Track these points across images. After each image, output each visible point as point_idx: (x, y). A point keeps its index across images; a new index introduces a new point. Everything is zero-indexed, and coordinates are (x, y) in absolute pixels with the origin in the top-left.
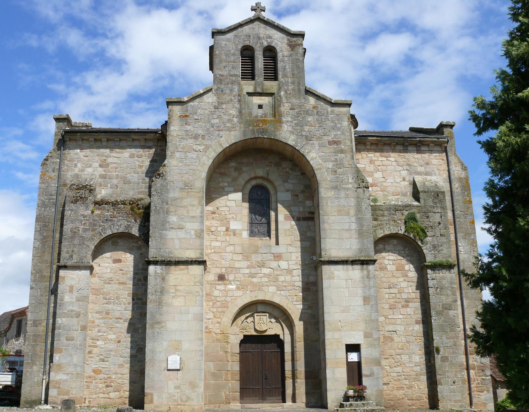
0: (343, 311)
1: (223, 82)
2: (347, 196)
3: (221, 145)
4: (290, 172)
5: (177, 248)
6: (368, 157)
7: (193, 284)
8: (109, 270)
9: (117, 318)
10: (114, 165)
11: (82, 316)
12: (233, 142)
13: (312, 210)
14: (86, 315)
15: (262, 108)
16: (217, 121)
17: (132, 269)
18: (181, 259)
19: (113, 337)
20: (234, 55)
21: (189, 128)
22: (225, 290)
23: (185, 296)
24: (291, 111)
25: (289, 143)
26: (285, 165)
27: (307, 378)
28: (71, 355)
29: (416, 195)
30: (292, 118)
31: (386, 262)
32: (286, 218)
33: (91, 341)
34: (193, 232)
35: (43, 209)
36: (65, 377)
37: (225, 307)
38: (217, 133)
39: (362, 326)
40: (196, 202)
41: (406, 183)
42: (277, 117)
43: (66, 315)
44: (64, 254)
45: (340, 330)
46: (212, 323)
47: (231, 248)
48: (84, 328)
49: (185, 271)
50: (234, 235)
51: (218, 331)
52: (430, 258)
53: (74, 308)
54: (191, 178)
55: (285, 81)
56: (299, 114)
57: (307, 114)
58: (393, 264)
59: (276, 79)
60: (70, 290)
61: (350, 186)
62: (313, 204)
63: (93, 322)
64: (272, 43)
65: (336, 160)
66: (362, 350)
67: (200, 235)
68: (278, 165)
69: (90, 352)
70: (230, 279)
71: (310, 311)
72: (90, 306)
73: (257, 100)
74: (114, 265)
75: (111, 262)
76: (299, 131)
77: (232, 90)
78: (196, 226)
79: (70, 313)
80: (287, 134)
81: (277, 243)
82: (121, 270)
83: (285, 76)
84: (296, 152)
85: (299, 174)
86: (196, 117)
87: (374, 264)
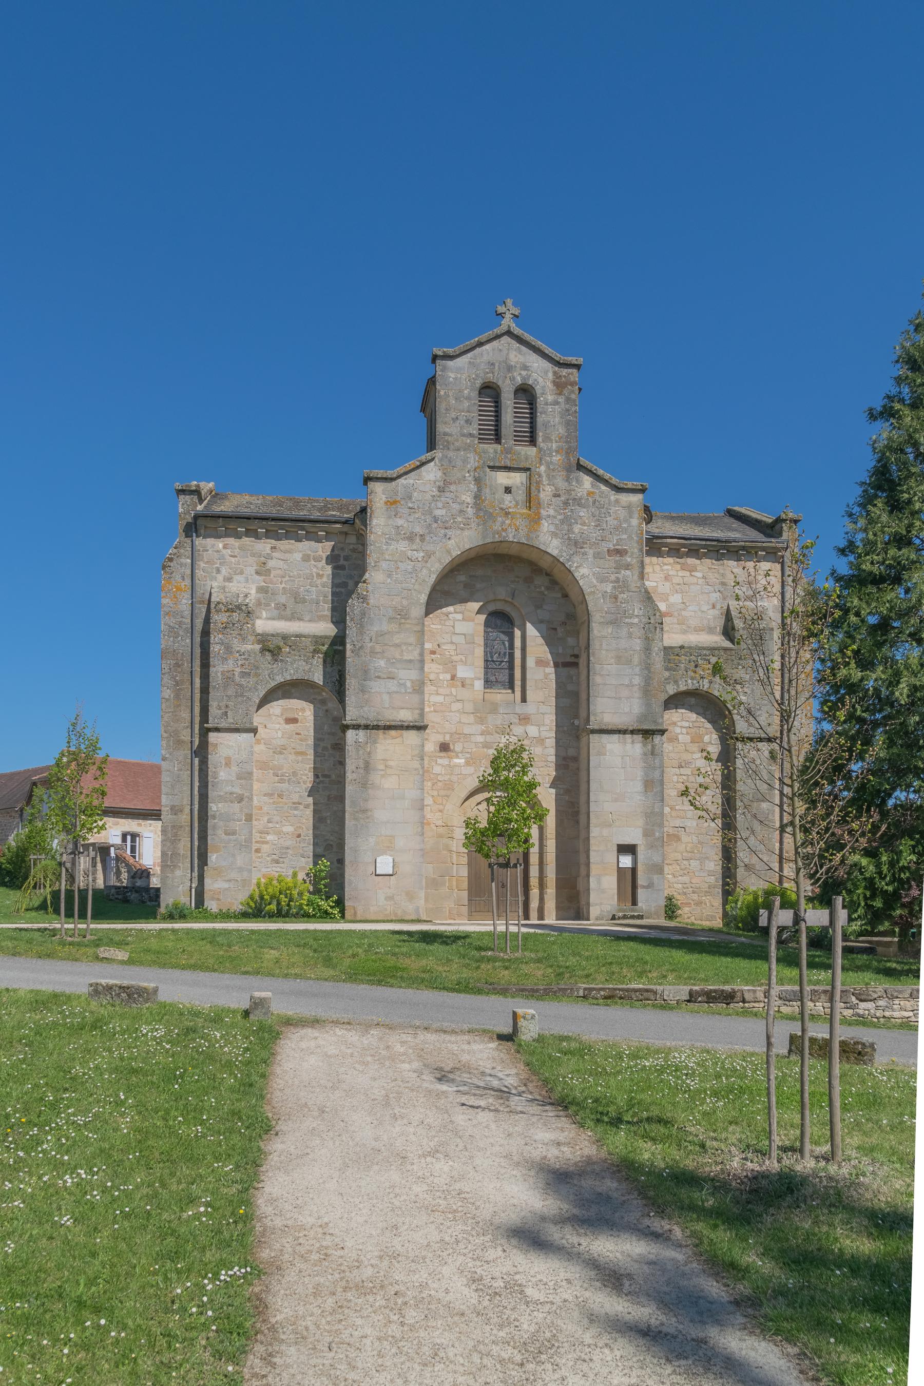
0: (616, 800)
1: (452, 447)
2: (630, 636)
3: (449, 552)
4: (546, 593)
5: (387, 706)
6: (662, 570)
7: (410, 757)
8: (280, 734)
9: (294, 803)
10: (279, 572)
11: (246, 800)
12: (467, 547)
13: (576, 652)
14: (251, 799)
15: (510, 492)
16: (443, 512)
17: (312, 732)
18: (393, 723)
19: (288, 829)
20: (468, 398)
21: (400, 522)
22: (449, 766)
23: (399, 775)
24: (554, 499)
25: (549, 551)
26: (540, 581)
27: (558, 888)
28: (234, 855)
29: (729, 631)
30: (555, 511)
31: (678, 730)
32: (540, 663)
33: (259, 835)
34: (409, 684)
35: (172, 639)
36: (226, 885)
37: (449, 789)
38: (443, 531)
39: (640, 822)
40: (412, 640)
41: (716, 612)
42: (533, 507)
43: (222, 799)
44: (214, 711)
45: (610, 826)
46: (431, 811)
47: (459, 706)
48: (249, 818)
49: (398, 740)
50: (463, 686)
51: (440, 823)
52: (741, 727)
53: (234, 790)
54: (405, 602)
55: (547, 449)
56: (566, 503)
57: (578, 505)
58: (687, 733)
59: (533, 441)
60: (226, 764)
61: (636, 620)
62: (578, 643)
63: (261, 808)
64: (528, 379)
65: (617, 580)
66: (641, 851)
67: (419, 688)
68: (528, 580)
69: (258, 851)
70: (456, 749)
71: (567, 798)
72: (256, 786)
73: (503, 478)
74: (288, 726)
75: (283, 722)
76: (564, 532)
77: (465, 461)
78: (413, 674)
79: (228, 796)
80: (550, 541)
81: (524, 700)
82: (297, 734)
83: (547, 439)
84: (559, 564)
85: (560, 595)
86: (410, 505)
87: (662, 735)
